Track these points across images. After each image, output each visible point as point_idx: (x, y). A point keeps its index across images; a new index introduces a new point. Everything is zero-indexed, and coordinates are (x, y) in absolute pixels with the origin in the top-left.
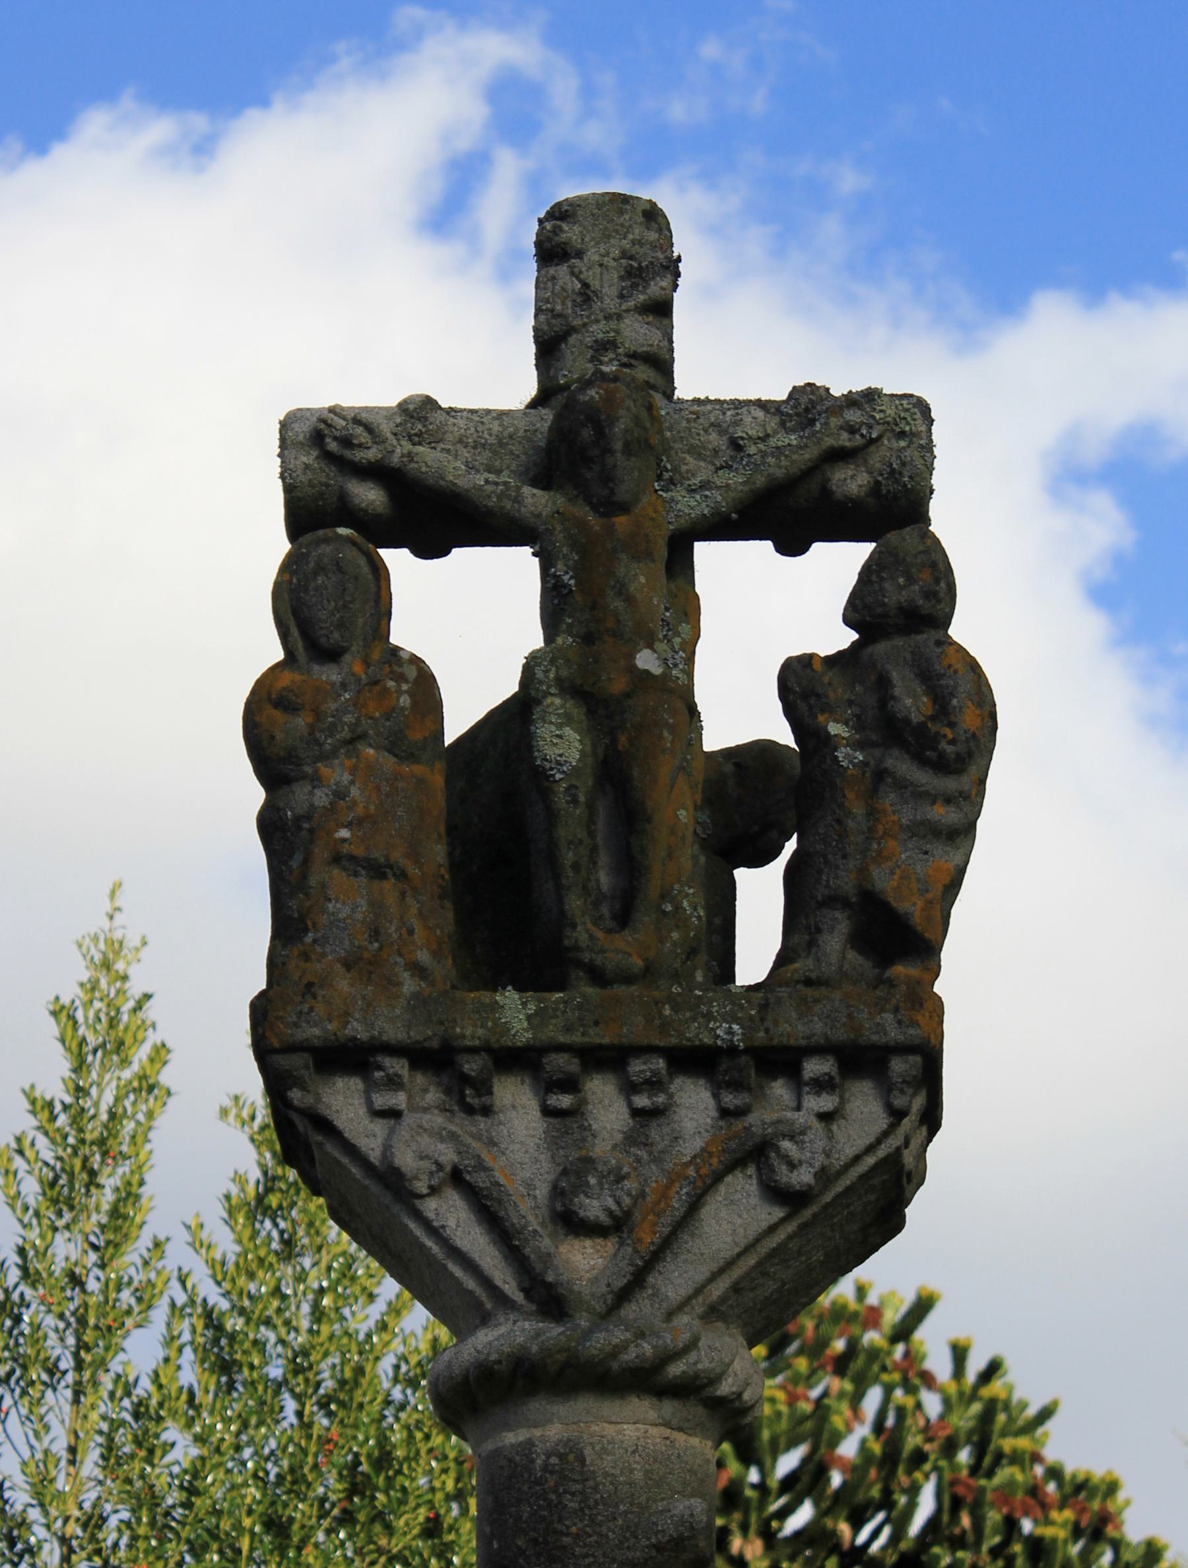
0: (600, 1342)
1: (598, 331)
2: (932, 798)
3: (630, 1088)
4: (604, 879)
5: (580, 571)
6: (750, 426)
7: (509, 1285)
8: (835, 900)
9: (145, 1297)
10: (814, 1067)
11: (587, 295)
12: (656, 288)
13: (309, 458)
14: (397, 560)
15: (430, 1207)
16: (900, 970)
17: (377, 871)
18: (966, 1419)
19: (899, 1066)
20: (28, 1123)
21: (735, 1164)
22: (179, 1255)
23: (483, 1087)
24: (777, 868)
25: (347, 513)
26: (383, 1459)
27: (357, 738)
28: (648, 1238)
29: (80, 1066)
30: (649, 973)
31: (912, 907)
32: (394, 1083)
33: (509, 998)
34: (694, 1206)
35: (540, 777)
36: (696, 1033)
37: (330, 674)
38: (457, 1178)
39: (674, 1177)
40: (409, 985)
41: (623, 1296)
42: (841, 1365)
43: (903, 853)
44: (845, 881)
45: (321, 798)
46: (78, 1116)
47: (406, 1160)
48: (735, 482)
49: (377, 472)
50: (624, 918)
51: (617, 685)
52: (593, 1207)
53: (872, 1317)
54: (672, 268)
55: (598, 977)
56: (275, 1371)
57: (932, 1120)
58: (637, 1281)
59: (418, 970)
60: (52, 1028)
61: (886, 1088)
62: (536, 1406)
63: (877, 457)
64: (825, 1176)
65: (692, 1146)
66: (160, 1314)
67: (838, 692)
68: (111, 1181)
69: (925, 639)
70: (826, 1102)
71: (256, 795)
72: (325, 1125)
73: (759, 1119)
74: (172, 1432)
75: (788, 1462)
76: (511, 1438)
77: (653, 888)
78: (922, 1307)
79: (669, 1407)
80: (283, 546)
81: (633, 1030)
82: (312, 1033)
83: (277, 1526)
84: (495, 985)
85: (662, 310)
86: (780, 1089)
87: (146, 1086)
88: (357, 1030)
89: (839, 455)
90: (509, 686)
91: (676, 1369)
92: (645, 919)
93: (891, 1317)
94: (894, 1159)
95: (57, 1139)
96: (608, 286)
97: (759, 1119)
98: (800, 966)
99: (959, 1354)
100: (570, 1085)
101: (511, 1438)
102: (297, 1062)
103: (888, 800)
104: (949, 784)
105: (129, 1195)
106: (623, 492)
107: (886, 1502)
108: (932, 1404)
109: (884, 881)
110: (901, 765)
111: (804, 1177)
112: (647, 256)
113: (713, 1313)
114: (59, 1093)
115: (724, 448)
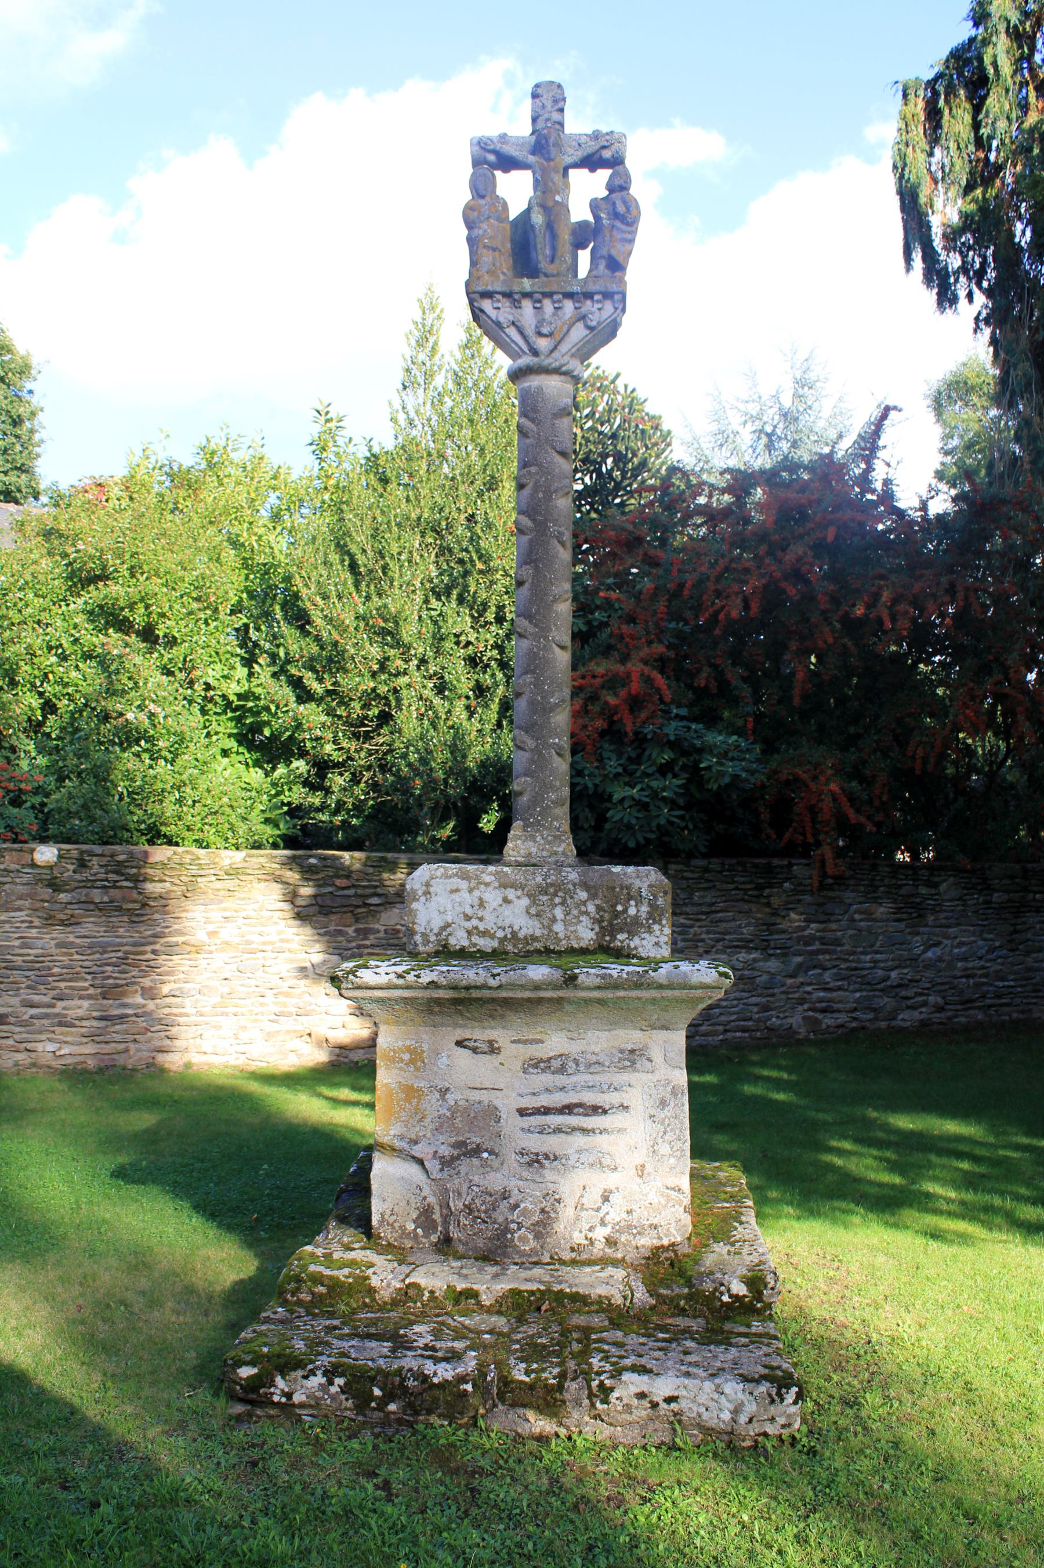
0: (546, 362)
1: (546, 116)
2: (625, 232)
3: (554, 302)
4: (548, 252)
5: (542, 176)
6: (583, 139)
7: (526, 349)
8: (602, 257)
9: (440, 368)
10: (597, 297)
11: (543, 107)
12: (560, 105)
13: (477, 148)
14: (498, 173)
15: (507, 330)
16: (617, 274)
17: (494, 250)
18: (627, 402)
19: (616, 297)
20: (412, 327)
21: (579, 320)
22: (447, 358)
23: (519, 302)
24: (588, 251)
25: (486, 162)
26: (494, 406)
27: (489, 217)
28: (558, 338)
29: (424, 313)
30: (558, 275)
31: (620, 259)
32: (498, 301)
33: (525, 280)
34: (568, 331)
35: (532, 227)
36: (569, 289)
37: (482, 202)
38: (513, 323)
39: (564, 323)
40: (502, 277)
41: (552, 351)
42: (599, 389)
43: (619, 246)
44: (604, 252)
45: (481, 232)
46: (424, 325)
47: (501, 319)
48: (579, 155)
49: (494, 152)
50: (552, 261)
51: (550, 204)
52: (545, 330)
53: (606, 378)
54: (564, 100)
55: (546, 275)
56: (470, 385)
57: (624, 310)
58: (555, 348)
59: (504, 274)
60: (417, 304)
61: (614, 303)
62: (532, 377)
63: (613, 148)
64: (599, 323)
65: (568, 316)
66: (443, 371)
67: (603, 206)
68: (431, 340)
69: (624, 193)
70: (599, 306)
71: (465, 232)
72: (482, 311)
73: (583, 310)
74: (447, 399)
75: (586, 411)
76: (526, 385)
77: (559, 254)
78: (618, 376)
79: (563, 378)
80: (471, 170)
81: (554, 288)
82: (479, 289)
83: (471, 421)
84: (522, 277)
85: (562, 110)
86: (589, 303)
87: (439, 318)
88: (490, 288)
89: (604, 147)
90: (525, 206)
91: (564, 369)
92: (557, 261)
93: (611, 378)
94: (615, 320)
95: (419, 330)
96: (549, 104)
97: (583, 310)
98: (594, 273)
99: (626, 387)
100: (539, 301)
101: (526, 385)
102: (476, 296)
103: (615, 233)
104: (629, 229)
105: (436, 343)
106: (552, 156)
107: (609, 421)
108: (619, 398)
109: (613, 252)
110: (618, 224)
111: (594, 323)
112: (558, 97)
113: (573, 356)
114: (420, 320)
115: (467, 899)
